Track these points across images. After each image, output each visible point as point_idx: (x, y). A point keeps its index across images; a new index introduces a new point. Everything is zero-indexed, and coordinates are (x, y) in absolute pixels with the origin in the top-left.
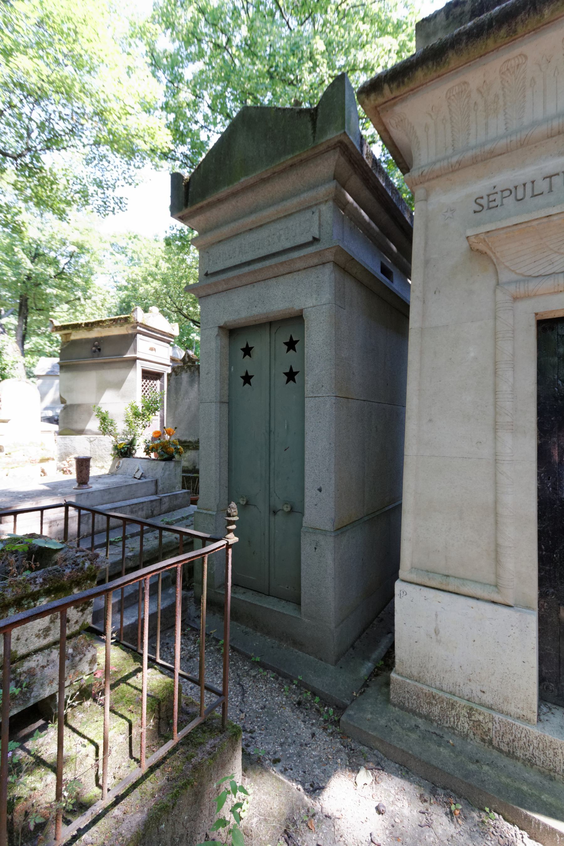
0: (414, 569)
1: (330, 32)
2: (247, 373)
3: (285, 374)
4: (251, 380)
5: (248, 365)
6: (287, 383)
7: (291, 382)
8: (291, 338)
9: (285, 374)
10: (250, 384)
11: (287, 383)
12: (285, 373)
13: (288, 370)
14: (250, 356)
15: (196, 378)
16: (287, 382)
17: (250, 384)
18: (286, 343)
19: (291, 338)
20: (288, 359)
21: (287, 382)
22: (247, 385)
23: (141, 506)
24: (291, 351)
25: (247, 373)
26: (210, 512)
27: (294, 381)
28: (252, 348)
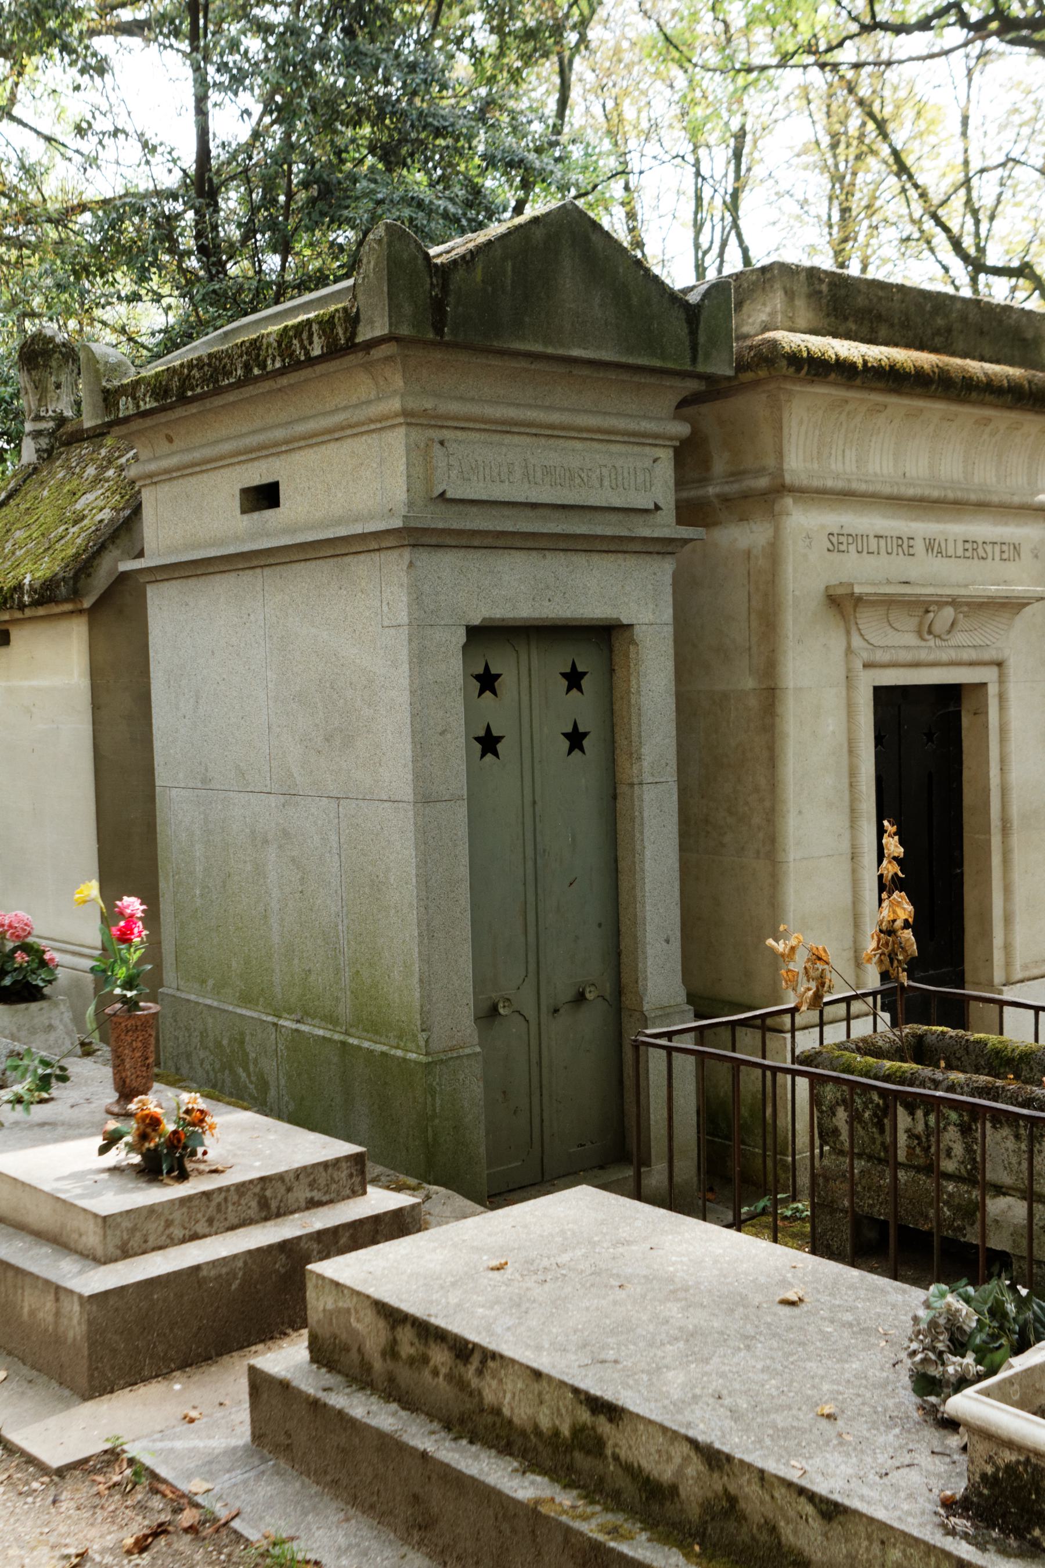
0: (1025, 967)
1: (435, 168)
2: (488, 729)
3: (565, 735)
4: (500, 747)
5: (498, 713)
6: (569, 753)
7: (577, 753)
8: (574, 665)
9: (565, 735)
10: (496, 754)
11: (569, 753)
12: (564, 734)
13: (569, 729)
14: (494, 693)
15: (852, 622)
16: (570, 752)
17: (496, 754)
18: (564, 675)
19: (574, 665)
20: (582, 708)
21: (570, 752)
22: (489, 757)
23: (821, 1181)
24: (575, 692)
25: (488, 729)
26: (468, 1051)
27: (583, 751)
28: (499, 676)
